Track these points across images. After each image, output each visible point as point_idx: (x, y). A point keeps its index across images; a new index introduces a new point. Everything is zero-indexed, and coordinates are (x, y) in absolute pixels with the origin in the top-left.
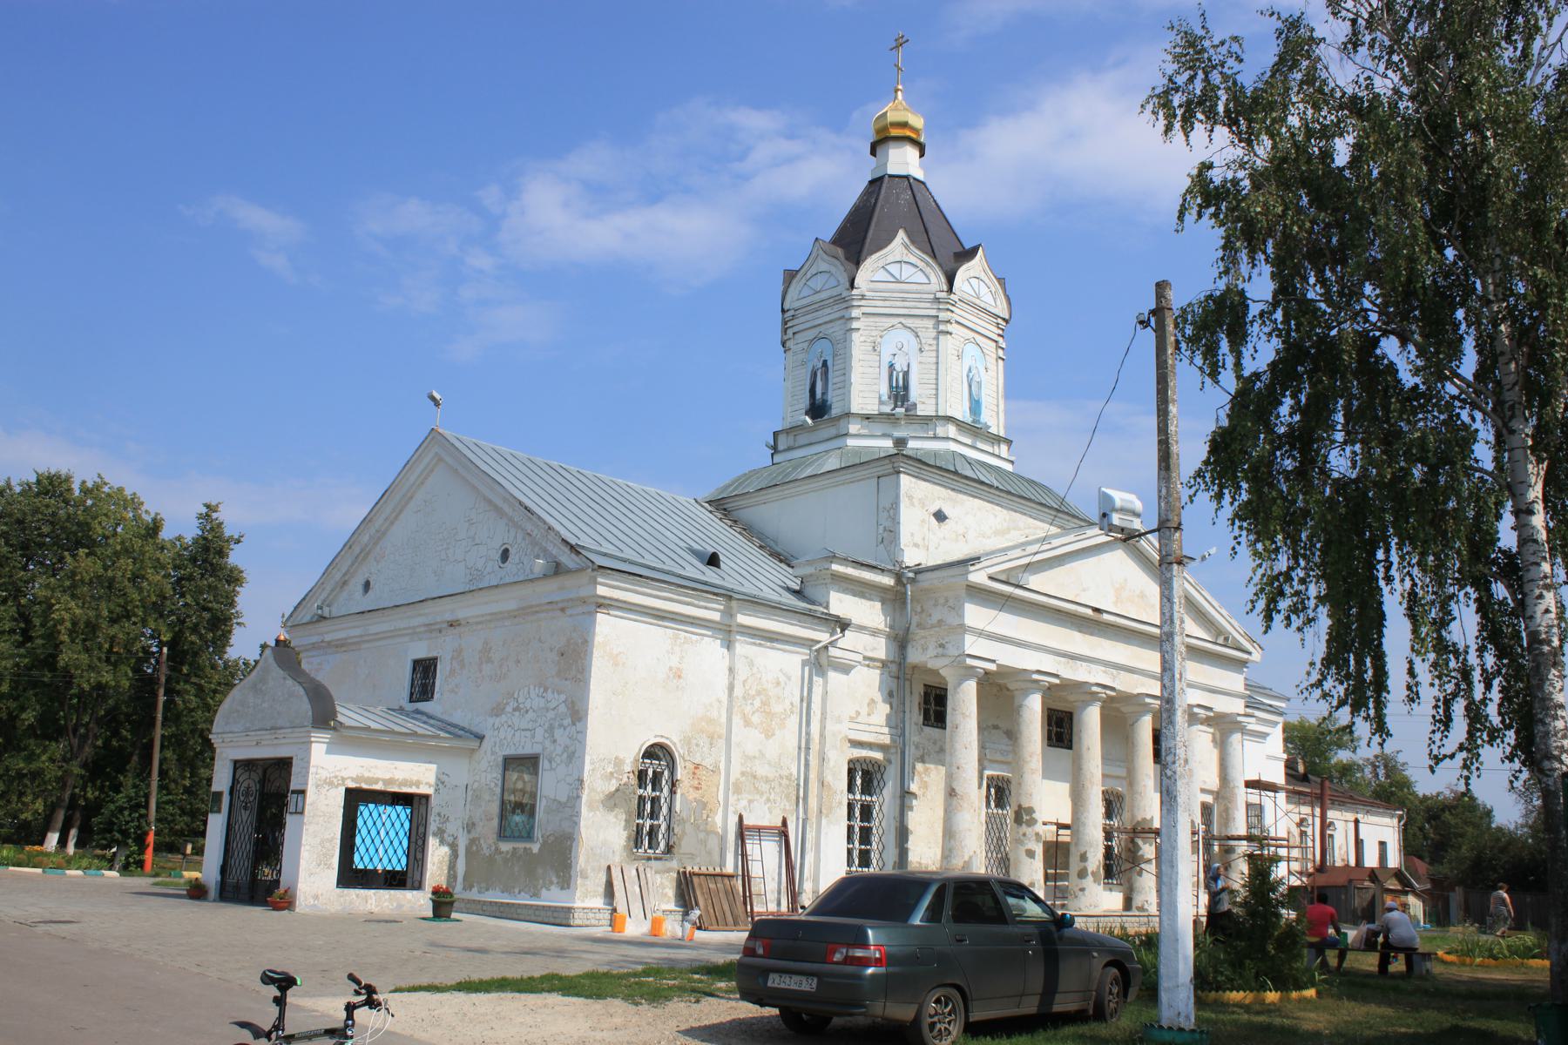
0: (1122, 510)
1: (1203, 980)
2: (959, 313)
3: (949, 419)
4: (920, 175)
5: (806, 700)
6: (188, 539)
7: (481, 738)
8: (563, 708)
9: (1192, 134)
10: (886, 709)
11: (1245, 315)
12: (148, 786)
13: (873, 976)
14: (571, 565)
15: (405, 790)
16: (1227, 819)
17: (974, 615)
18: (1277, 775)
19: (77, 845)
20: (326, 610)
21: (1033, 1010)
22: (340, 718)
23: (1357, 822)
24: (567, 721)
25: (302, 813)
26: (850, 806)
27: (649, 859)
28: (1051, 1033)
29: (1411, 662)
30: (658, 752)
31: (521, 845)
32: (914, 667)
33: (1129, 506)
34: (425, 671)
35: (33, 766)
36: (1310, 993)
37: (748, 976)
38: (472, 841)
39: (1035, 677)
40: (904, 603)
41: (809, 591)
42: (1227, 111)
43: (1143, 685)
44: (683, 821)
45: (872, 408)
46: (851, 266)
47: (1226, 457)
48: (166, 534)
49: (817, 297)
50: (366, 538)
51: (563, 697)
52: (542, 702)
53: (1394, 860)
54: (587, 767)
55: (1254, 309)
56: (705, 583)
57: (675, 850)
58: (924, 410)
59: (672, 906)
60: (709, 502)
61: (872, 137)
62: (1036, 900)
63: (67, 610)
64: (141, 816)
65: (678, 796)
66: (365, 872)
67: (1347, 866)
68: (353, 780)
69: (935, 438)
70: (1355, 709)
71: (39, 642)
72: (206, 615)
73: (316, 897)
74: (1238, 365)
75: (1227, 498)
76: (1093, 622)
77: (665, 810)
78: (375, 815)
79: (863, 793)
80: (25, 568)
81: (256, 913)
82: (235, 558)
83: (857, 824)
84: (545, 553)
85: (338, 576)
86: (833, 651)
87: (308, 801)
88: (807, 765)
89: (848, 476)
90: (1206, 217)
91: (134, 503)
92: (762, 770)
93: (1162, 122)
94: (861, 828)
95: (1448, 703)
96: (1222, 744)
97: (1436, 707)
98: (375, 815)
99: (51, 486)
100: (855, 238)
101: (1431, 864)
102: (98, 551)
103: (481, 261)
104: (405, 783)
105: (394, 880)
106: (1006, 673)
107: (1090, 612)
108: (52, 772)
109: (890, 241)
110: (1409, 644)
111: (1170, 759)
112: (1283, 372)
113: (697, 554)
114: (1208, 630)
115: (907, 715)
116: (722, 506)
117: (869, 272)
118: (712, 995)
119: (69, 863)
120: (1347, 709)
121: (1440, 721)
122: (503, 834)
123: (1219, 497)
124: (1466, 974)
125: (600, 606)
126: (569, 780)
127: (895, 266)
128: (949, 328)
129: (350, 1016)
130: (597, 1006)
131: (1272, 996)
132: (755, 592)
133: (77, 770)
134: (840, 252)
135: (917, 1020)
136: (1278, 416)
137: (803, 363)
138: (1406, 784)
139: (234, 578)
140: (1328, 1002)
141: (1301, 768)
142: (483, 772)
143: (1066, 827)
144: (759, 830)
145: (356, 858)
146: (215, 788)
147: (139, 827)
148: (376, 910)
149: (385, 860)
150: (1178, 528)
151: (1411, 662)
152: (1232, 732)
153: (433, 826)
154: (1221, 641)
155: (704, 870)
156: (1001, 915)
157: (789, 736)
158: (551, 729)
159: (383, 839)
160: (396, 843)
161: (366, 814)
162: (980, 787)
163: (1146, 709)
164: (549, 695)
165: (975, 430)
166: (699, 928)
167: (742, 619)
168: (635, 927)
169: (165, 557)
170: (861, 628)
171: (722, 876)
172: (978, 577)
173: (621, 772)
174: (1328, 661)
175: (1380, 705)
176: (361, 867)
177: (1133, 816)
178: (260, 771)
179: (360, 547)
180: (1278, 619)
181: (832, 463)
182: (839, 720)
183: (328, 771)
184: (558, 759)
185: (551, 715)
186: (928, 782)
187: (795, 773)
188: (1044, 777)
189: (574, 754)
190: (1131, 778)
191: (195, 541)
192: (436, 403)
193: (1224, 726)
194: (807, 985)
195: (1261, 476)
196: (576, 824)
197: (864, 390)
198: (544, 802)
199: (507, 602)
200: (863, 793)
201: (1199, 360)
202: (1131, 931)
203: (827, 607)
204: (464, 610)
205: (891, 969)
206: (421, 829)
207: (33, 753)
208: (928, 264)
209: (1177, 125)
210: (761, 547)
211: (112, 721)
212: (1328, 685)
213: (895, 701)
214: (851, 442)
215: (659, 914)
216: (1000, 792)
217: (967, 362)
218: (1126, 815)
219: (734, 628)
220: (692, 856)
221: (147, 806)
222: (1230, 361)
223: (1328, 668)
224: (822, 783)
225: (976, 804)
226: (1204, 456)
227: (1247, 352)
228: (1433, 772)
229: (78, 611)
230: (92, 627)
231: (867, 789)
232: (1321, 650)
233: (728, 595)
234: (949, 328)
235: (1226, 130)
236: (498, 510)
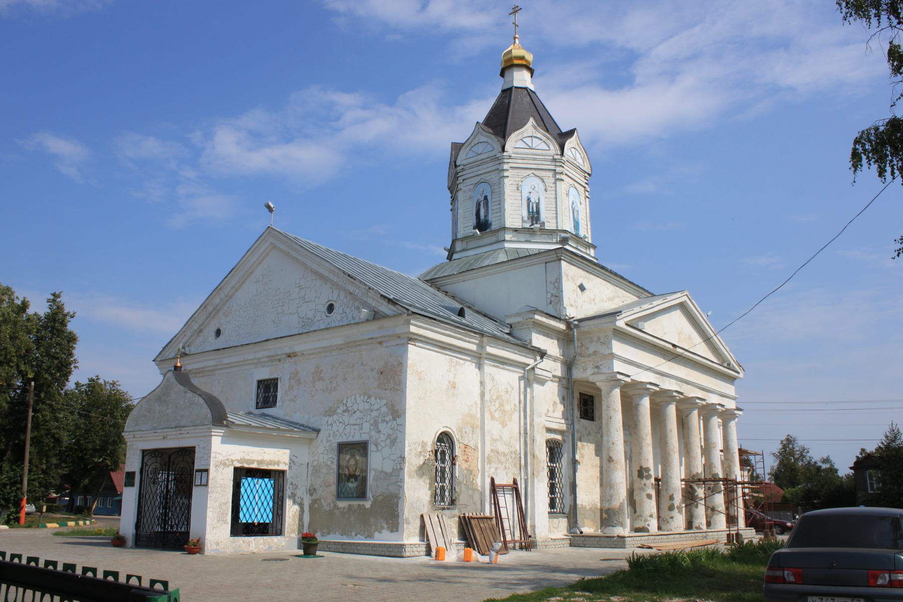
2: (567, 169)
4: (532, 87)
7: (318, 431)
8: (384, 409)
12: (23, 469)
14: (389, 312)
17: (618, 348)
20: (187, 349)
25: (206, 485)
31: (355, 503)
38: (314, 502)
39: (649, 386)
44: (460, 483)
45: (518, 224)
48: (30, 311)
49: (479, 158)
50: (217, 301)
51: (384, 402)
52: (367, 406)
54: (407, 449)
57: (457, 502)
64: (18, 489)
65: (457, 466)
68: (238, 461)
73: (217, 544)
76: (671, 354)
81: (176, 557)
82: (71, 326)
84: (366, 305)
85: (196, 327)
87: (211, 476)
92: (502, 448)
100: (499, 123)
104: (260, 462)
106: (635, 384)
107: (670, 346)
114: (718, 359)
117: (513, 142)
125: (410, 339)
126: (393, 457)
128: (563, 177)
137: (471, 198)
139: (72, 339)
142: (324, 454)
144: (503, 487)
147: (16, 496)
149: (259, 516)
153: (288, 492)
154: (725, 365)
157: (514, 427)
158: (376, 424)
159: (257, 503)
161: (246, 485)
164: (373, 400)
165: (577, 238)
167: (490, 350)
172: (621, 323)
173: (425, 451)
182: (540, 416)
183: (223, 455)
184: (383, 444)
185: (375, 414)
186: (586, 452)
189: (396, 439)
197: (514, 214)
198: (373, 473)
199: (337, 338)
204: (298, 346)
206: (281, 494)
208: (548, 138)
214: (507, 245)
217: (571, 199)
220: (466, 506)
221: (21, 482)
234: (563, 177)
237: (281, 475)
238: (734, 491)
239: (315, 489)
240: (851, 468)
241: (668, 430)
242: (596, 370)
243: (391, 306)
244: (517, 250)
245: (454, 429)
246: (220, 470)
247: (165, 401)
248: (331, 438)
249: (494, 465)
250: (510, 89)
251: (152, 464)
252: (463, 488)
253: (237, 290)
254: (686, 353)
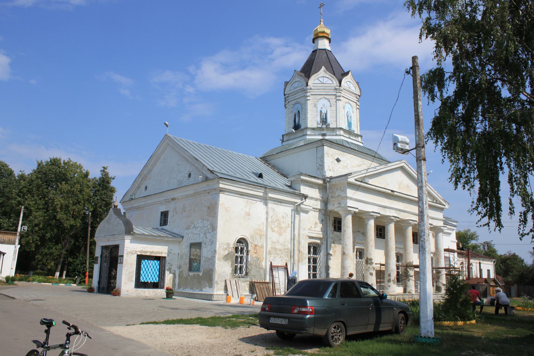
0: (402, 142)
1: (436, 318)
2: (343, 93)
3: (341, 129)
4: (329, 49)
5: (293, 223)
6: (98, 178)
7: (183, 237)
8: (209, 226)
9: (422, 15)
10: (321, 225)
11: (444, 77)
12: (86, 257)
13: (309, 318)
14: (211, 177)
15: (160, 255)
16: (438, 261)
17: (350, 193)
18: (454, 247)
19: (66, 276)
21: (372, 330)
22: (135, 231)
23: (480, 263)
24: (211, 231)
25: (122, 263)
26: (309, 259)
27: (240, 277)
28: (379, 339)
29: (510, 200)
30: (242, 241)
31: (196, 273)
32: (330, 211)
33: (405, 141)
34: (165, 215)
35: (50, 251)
36: (474, 322)
37: (263, 318)
38: (181, 272)
39: (372, 214)
40: (326, 190)
41: (294, 186)
42: (435, 6)
43: (409, 216)
45: (315, 126)
46: (306, 79)
47: (439, 127)
48: (90, 177)
51: (209, 222)
53: (492, 276)
54: (217, 246)
55: (447, 76)
56: (257, 183)
57: (249, 274)
58: (331, 126)
59: (248, 293)
60: (261, 158)
61: (313, 37)
62: (373, 289)
63: (59, 201)
64: (84, 267)
65: (249, 256)
67: (477, 278)
68: (139, 252)
69: (336, 135)
70: (490, 217)
71: (51, 211)
72: (104, 202)
73: (128, 291)
74: (441, 95)
75: (439, 143)
76: (391, 195)
77: (245, 260)
78: (147, 263)
79: (313, 254)
80: (47, 188)
82: (113, 184)
83: (312, 265)
84: (202, 174)
85: (137, 185)
86: (302, 206)
87: (124, 259)
88: (294, 245)
89: (306, 147)
90: (429, 38)
91: (80, 167)
92: (278, 247)
93: (411, 10)
94: (313, 266)
95: (525, 214)
96: (436, 237)
97: (521, 216)
98: (147, 263)
99: (55, 162)
100: (308, 70)
101: (503, 277)
102: (69, 182)
103: (190, 89)
104: (157, 253)
105: (155, 286)
107: (390, 192)
108: (56, 253)
109: (319, 70)
110: (510, 193)
111: (422, 234)
112: (459, 94)
113: (255, 174)
115: (328, 228)
116: (265, 159)
117: (313, 81)
118: (255, 325)
119: (60, 281)
120: (487, 217)
121: (522, 221)
122: (190, 269)
123: (436, 142)
124: (526, 314)
126: (212, 250)
127: (321, 78)
128: (340, 98)
129: (68, 339)
130: (211, 329)
131: (460, 323)
132: (275, 186)
133: (64, 252)
134: (303, 74)
135: (327, 335)
136: (458, 110)
137: (292, 112)
138: (494, 251)
140: (480, 324)
141: (461, 246)
142: (184, 249)
143: (383, 265)
144: (278, 267)
145: (141, 278)
146: (96, 255)
147: (84, 270)
148: (148, 295)
150: (423, 147)
151: (510, 200)
152: (439, 232)
153: (167, 267)
154: (435, 201)
155: (259, 281)
156: (359, 295)
157: (287, 235)
159: (150, 272)
160: (155, 273)
161: (144, 263)
162: (354, 252)
163: (410, 224)
164: (205, 222)
165: (349, 132)
166: (257, 301)
167: (270, 195)
168: (234, 301)
169: (90, 184)
170: (312, 198)
171: (265, 283)
172: (351, 180)
173: (229, 248)
174: (479, 200)
175: (499, 216)
176: (143, 281)
177: (406, 261)
178: (110, 250)
179: (143, 176)
180: (460, 186)
181: (302, 143)
182: (305, 230)
183: (131, 249)
185: (205, 228)
186: (336, 250)
187: (290, 247)
188: (376, 248)
189: (213, 242)
190: (405, 248)
191: (100, 179)
192: (167, 126)
193: (436, 230)
194: (284, 322)
195: (452, 132)
196: (214, 265)
197: (312, 120)
199: (190, 191)
200: (313, 254)
201: (427, 94)
202: (407, 300)
203: (300, 191)
205: (316, 316)
206: (163, 268)
207: (50, 247)
208: (332, 77)
209: (417, 12)
210: (278, 172)
211: (75, 237)
212: (480, 209)
213: (324, 222)
214: (308, 137)
215: (243, 296)
216: (360, 254)
218: (404, 261)
219: (268, 198)
220: (255, 276)
221: (86, 263)
222: (438, 94)
223: (479, 202)
224: (299, 251)
225: (352, 257)
226: (430, 127)
227: (444, 91)
228: (521, 240)
229: (62, 202)
230: (67, 206)
231: (315, 253)
232: (476, 196)
233: (265, 187)
234: (340, 98)
235: (435, 12)
236: (187, 160)
238: (439, 272)
241: (389, 238)
242: (339, 205)
245: (248, 237)
246: (129, 256)
249: (272, 255)
250: (316, 50)
252: (253, 267)
253: (154, 167)
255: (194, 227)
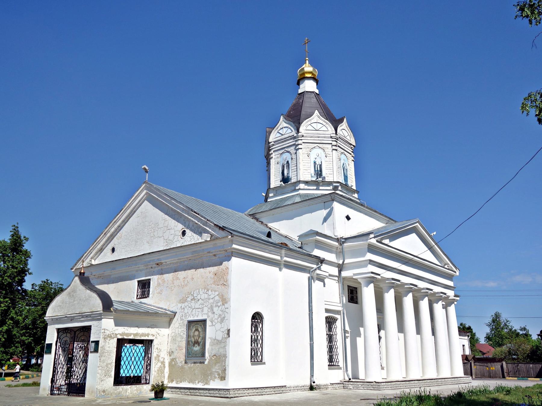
8: (217, 298)
38: (172, 360)
45: (309, 179)
51: (217, 293)
58: (327, 179)
66: (127, 377)
68: (120, 335)
82: (27, 246)
126: (222, 330)
145: (122, 371)
149: (134, 371)
176: (124, 375)
185: (211, 301)
191: (11, 242)
192: (147, 172)
214: (301, 192)
217: (342, 162)
237: (150, 342)
239: (172, 352)
240: (538, 335)
243: (221, 231)
244: (307, 195)
246: (107, 341)
247: (73, 295)
248: (184, 318)
251: (67, 338)
254: (415, 258)
255: (193, 299)
